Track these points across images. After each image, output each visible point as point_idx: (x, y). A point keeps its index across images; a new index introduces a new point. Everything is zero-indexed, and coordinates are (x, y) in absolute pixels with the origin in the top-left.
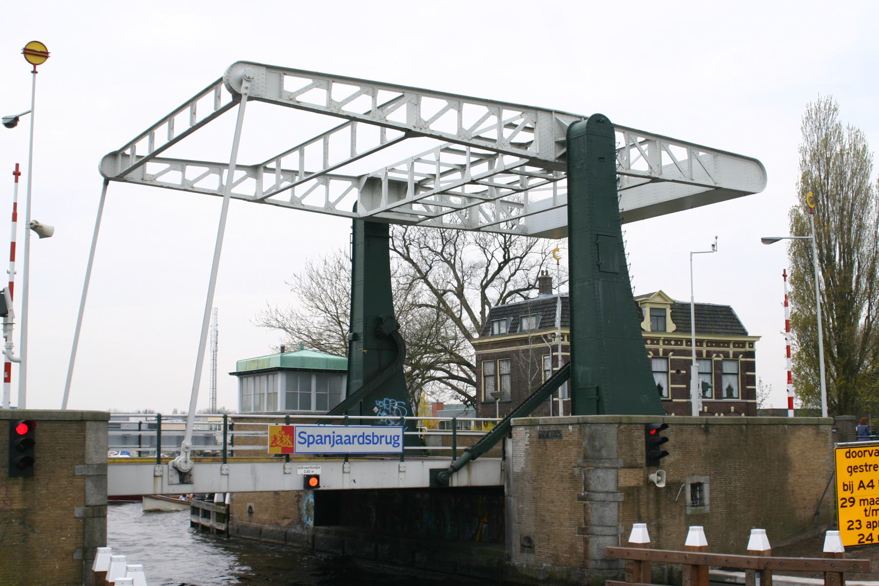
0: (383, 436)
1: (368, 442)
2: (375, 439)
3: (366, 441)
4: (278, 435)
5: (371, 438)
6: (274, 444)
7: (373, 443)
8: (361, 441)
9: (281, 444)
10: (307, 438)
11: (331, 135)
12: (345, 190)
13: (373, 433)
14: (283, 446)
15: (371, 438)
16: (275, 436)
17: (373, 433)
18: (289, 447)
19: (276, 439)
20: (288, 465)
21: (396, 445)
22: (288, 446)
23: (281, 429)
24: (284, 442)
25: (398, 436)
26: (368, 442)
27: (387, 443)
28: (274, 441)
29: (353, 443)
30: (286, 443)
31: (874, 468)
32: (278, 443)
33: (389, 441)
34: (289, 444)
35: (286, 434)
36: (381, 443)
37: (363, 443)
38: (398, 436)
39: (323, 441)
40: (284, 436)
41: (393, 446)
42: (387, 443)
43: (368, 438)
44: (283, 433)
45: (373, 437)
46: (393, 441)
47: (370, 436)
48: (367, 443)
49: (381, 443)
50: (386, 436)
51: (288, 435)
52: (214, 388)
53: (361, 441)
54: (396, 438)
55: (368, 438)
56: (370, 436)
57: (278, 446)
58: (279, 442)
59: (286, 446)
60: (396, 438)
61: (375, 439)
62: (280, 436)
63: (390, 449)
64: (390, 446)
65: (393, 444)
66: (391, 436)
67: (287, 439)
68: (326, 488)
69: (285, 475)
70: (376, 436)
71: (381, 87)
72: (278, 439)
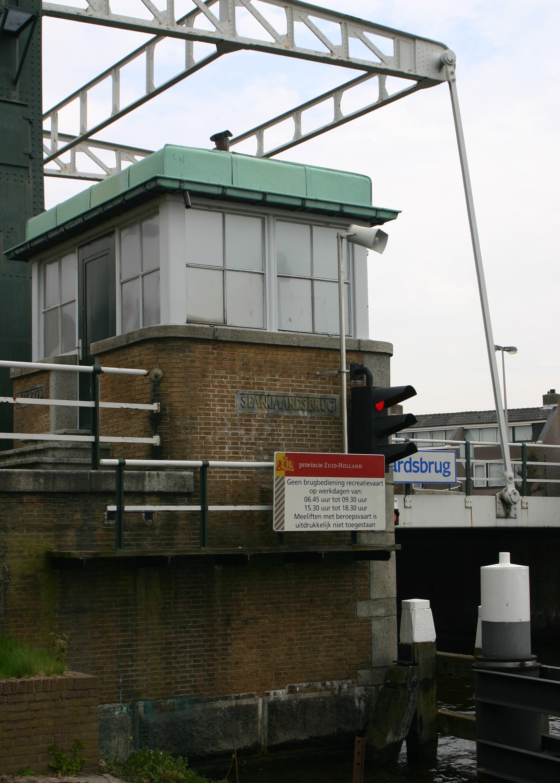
0: (433, 463)
1: (416, 469)
2: (424, 466)
3: (413, 468)
4: (282, 460)
5: (419, 465)
6: (279, 468)
7: (422, 471)
8: (408, 468)
9: (285, 468)
10: (412, 467)
11: (265, 131)
12: (311, 165)
13: (421, 459)
14: (286, 470)
15: (419, 465)
16: (280, 461)
17: (421, 459)
18: (291, 470)
19: (280, 463)
20: (409, 498)
21: (446, 474)
22: (290, 470)
23: (284, 456)
24: (287, 466)
25: (449, 463)
26: (416, 469)
27: (437, 472)
28: (279, 466)
29: (399, 471)
30: (288, 467)
31: (357, 483)
32: (282, 467)
33: (438, 469)
34: (291, 468)
35: (289, 460)
36: (430, 472)
37: (410, 471)
38: (449, 463)
39: (397, 468)
40: (287, 461)
41: (444, 475)
42: (437, 472)
43: (416, 464)
44: (287, 458)
45: (422, 463)
46: (443, 469)
47: (418, 463)
48: (414, 471)
49: (430, 472)
50: (436, 463)
51: (291, 461)
52: (504, 414)
53: (408, 468)
54: (446, 466)
55: (416, 464)
56: (418, 463)
57: (282, 469)
58: (283, 466)
59: (289, 470)
60: (446, 466)
61: (424, 466)
62: (284, 461)
63: (439, 478)
64: (440, 474)
65: (443, 472)
66: (441, 463)
67: (290, 464)
68: (407, 526)
69: (406, 509)
70: (425, 462)
71: (138, 153)
72: (283, 464)
